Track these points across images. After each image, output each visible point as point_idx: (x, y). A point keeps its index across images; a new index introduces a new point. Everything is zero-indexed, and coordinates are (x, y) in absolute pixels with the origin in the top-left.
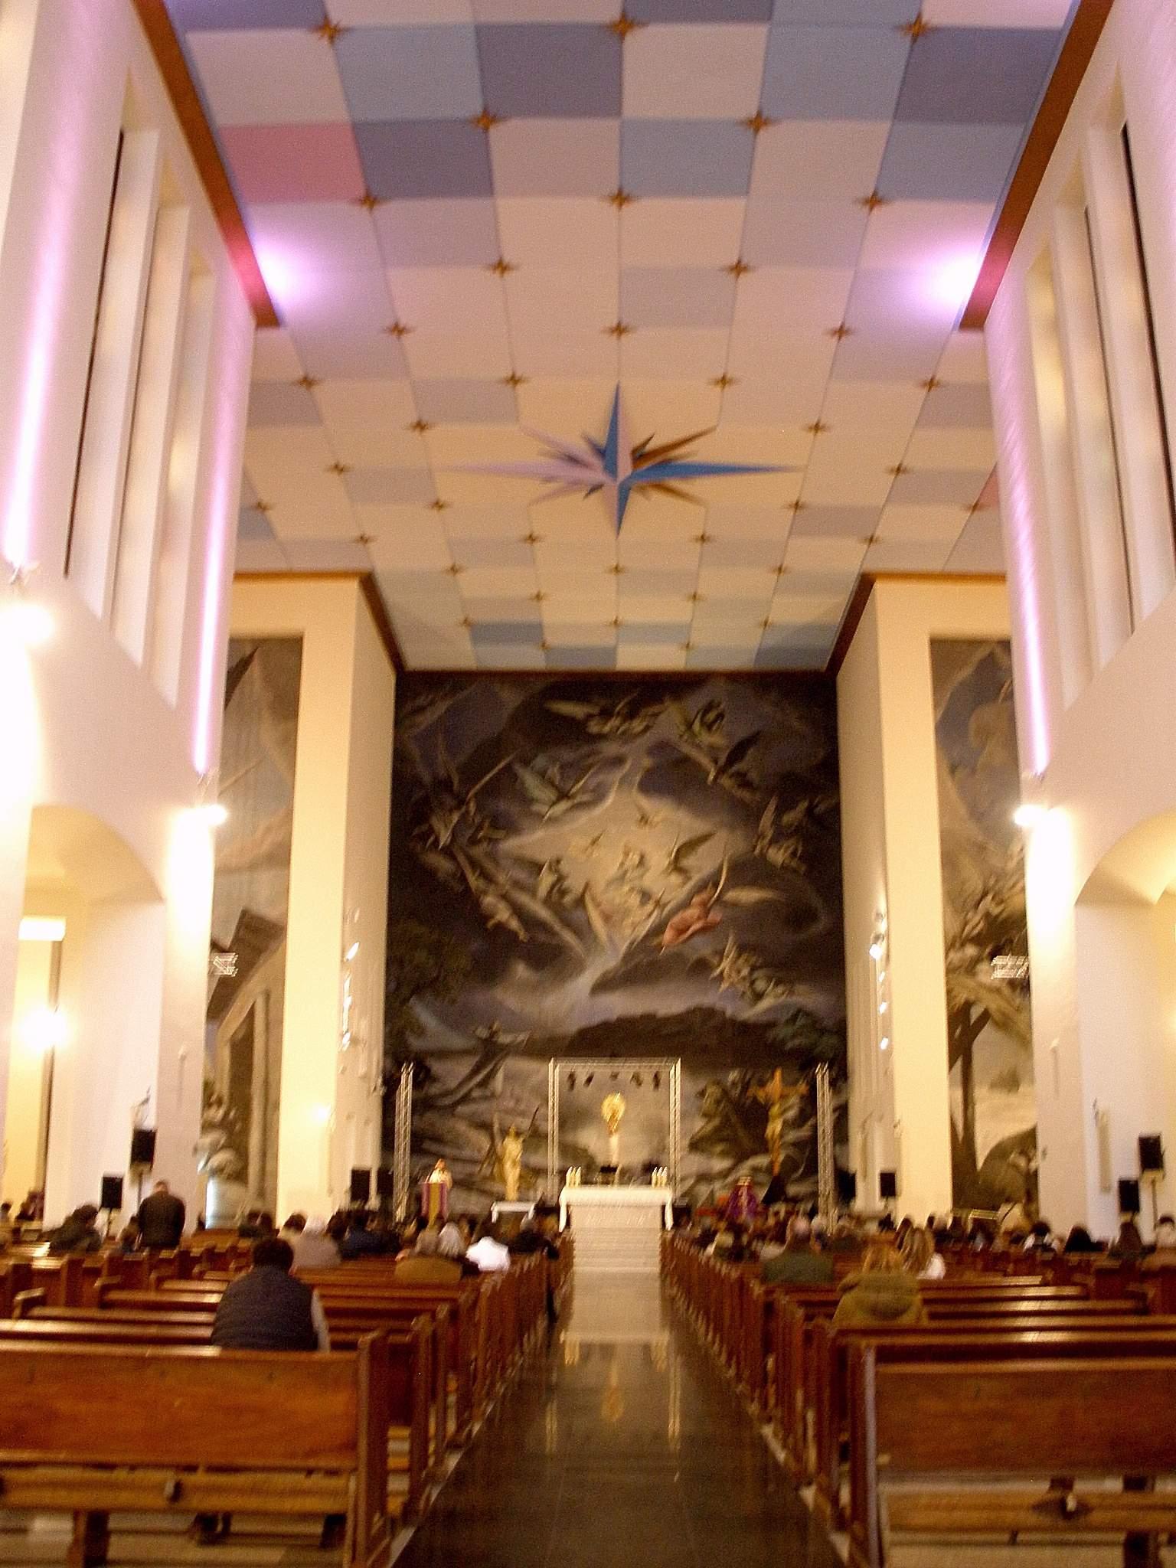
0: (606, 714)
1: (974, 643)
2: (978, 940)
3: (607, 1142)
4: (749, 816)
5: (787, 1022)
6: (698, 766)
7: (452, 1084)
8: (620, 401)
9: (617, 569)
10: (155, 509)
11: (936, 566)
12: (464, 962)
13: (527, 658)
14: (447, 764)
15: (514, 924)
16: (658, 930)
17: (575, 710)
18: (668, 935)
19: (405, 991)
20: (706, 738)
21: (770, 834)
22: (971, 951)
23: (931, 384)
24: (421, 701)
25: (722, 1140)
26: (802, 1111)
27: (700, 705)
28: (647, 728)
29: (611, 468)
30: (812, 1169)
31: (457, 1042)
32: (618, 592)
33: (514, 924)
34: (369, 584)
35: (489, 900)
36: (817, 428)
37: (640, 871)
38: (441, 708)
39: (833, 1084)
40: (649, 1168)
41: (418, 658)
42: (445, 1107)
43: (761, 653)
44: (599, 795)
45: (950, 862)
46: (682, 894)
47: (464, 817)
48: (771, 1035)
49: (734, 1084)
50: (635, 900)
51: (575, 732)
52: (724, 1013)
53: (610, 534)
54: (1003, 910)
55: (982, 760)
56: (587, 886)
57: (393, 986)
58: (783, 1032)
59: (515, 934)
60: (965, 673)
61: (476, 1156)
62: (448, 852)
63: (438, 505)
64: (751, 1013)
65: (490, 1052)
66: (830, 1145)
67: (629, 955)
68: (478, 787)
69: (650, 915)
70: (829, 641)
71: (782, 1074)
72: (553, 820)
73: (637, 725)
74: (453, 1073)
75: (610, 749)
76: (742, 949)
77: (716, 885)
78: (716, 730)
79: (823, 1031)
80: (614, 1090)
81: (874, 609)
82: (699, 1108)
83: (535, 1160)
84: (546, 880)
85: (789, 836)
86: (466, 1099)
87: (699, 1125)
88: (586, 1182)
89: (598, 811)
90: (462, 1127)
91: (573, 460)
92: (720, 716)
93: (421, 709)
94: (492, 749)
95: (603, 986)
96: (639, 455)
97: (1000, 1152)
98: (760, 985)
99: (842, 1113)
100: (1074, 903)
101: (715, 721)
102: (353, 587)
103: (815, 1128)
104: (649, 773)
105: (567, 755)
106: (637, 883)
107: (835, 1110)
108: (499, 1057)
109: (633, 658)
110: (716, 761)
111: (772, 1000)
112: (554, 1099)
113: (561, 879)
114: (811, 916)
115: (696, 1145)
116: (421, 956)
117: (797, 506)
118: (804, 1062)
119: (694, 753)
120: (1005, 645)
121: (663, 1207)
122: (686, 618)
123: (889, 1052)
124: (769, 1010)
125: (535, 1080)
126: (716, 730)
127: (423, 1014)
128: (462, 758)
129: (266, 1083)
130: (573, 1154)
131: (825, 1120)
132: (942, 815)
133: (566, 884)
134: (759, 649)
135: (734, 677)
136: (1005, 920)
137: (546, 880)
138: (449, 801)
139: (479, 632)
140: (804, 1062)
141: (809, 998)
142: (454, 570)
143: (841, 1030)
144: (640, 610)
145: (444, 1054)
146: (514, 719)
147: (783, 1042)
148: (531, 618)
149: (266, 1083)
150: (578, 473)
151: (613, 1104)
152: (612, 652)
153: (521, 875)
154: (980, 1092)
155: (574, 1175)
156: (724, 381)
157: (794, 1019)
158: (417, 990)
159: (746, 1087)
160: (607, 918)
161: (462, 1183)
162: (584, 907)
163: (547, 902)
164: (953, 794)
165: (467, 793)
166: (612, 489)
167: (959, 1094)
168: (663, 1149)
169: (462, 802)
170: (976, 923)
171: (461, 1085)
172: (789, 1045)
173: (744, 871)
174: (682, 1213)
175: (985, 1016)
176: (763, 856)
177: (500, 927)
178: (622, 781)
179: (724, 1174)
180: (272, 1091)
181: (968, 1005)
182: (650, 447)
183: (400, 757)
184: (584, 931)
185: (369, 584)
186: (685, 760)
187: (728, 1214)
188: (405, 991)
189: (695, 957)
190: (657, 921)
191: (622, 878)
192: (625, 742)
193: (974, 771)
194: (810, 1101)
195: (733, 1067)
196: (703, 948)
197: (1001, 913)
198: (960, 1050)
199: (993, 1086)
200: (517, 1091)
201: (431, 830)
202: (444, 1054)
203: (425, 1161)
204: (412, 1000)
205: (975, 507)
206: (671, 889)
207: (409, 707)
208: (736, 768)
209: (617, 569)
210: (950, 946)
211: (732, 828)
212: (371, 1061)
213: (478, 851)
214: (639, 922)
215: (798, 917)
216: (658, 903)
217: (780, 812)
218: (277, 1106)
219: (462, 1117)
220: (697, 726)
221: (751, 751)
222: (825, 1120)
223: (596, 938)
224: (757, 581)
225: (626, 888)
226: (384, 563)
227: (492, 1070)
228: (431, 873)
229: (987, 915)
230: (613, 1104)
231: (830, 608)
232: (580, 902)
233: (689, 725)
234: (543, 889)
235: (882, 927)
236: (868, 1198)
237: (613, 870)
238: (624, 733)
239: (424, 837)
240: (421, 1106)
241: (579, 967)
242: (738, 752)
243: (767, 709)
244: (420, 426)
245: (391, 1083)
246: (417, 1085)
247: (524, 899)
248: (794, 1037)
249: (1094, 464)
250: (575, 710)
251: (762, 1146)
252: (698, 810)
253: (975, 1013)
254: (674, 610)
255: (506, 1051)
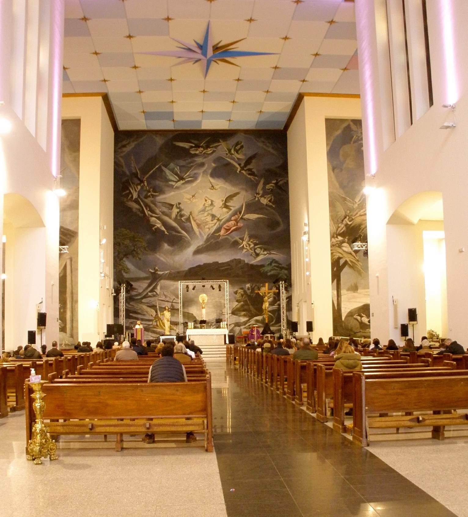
0: (197, 146)
1: (342, 121)
2: (343, 235)
3: (201, 311)
4: (253, 186)
5: (268, 264)
6: (234, 166)
7: (141, 291)
8: (210, 27)
9: (204, 91)
10: (342, 294)
11: (328, 91)
12: (144, 244)
13: (166, 125)
14: (135, 167)
15: (163, 228)
16: (218, 230)
17: (186, 145)
18: (222, 232)
19: (121, 255)
20: (236, 156)
21: (261, 192)
22: (340, 238)
23: (332, 22)
24: (124, 143)
25: (244, 311)
26: (274, 298)
27: (233, 144)
28: (214, 151)
29: (205, 54)
30: (278, 321)
31: (143, 275)
32: (204, 100)
33: (163, 228)
34: (106, 98)
35: (153, 219)
36: (286, 38)
37: (211, 207)
38: (133, 145)
39: (286, 289)
40: (219, 321)
41: (123, 126)
42: (137, 299)
43: (258, 123)
44: (195, 178)
45: (332, 205)
46: (227, 216)
47: (142, 187)
48: (262, 270)
49: (248, 289)
50: (209, 218)
51: (185, 153)
52: (245, 262)
53: (203, 78)
54: (352, 223)
55: (345, 166)
56: (191, 213)
57: (117, 254)
58: (267, 269)
59: (164, 232)
60: (339, 132)
61: (151, 318)
62: (136, 201)
63: (135, 67)
64: (254, 261)
65: (155, 278)
66: (285, 312)
67: (208, 240)
68: (148, 175)
69: (215, 224)
70: (285, 119)
71: (268, 285)
72: (177, 188)
73: (209, 151)
74: (141, 287)
75: (199, 160)
76: (251, 237)
77: (240, 213)
78: (240, 153)
79: (282, 268)
80: (204, 292)
81: (304, 107)
82: (235, 298)
83: (174, 319)
84: (175, 211)
85: (268, 194)
86: (145, 297)
87: (235, 304)
88: (195, 327)
89: (194, 184)
90: (145, 307)
91: (190, 50)
92: (242, 147)
93: (124, 146)
94: (153, 161)
95: (197, 252)
96: (216, 48)
97: (350, 314)
98: (258, 251)
99: (289, 299)
100: (386, 223)
101: (239, 149)
102: (100, 99)
103: (279, 305)
104: (215, 169)
105: (182, 162)
106: (210, 212)
107: (287, 299)
108: (158, 280)
109: (208, 125)
110: (240, 165)
111: (263, 256)
112: (181, 296)
113: (181, 210)
114: (277, 224)
115: (234, 313)
116: (127, 242)
117: (276, 68)
118: (275, 281)
119: (232, 161)
120: (358, 123)
121: (225, 336)
122: (230, 110)
123: (309, 276)
124: (262, 260)
125: (172, 288)
126: (240, 153)
127: (128, 264)
128: (141, 165)
129: (72, 293)
130: (188, 316)
131: (283, 303)
132: (329, 187)
133: (183, 212)
134: (258, 121)
135: (246, 132)
136: (353, 226)
137: (175, 211)
138: (137, 181)
139: (148, 115)
140: (275, 281)
141: (277, 256)
142: (140, 92)
143: (289, 268)
144: (212, 107)
145: (138, 279)
146: (161, 149)
147: (267, 272)
148: (168, 110)
149: (72, 293)
150: (192, 55)
151: (203, 297)
152: (200, 122)
153: (165, 209)
154: (343, 292)
155: (191, 324)
156: (251, 20)
157: (271, 264)
158: (126, 255)
159: (253, 290)
160: (198, 225)
161: (147, 329)
162: (190, 222)
163: (175, 220)
164: (334, 179)
165: (144, 178)
166: (204, 61)
167: (335, 292)
168: (222, 314)
169: (142, 182)
170: (342, 228)
171: (144, 291)
172: (269, 274)
173: (251, 207)
174: (232, 339)
175: (346, 263)
176: (259, 200)
177: (158, 229)
178: (204, 172)
179: (245, 323)
180: (74, 296)
181: (339, 258)
182: (220, 45)
183: (117, 164)
184: (190, 231)
185: (106, 98)
186: (229, 164)
187: (246, 338)
188: (121, 255)
189: (233, 240)
190: (219, 226)
191: (204, 210)
192: (205, 157)
193: (342, 170)
194: (277, 295)
195: (249, 282)
196: (236, 237)
197: (351, 224)
198: (336, 276)
199: (348, 290)
200: (165, 293)
201: (130, 193)
202: (138, 279)
203: (132, 320)
204: (124, 259)
205: (345, 69)
206: (224, 214)
207: (120, 145)
208: (248, 167)
209: (204, 91)
210: (332, 237)
211: (246, 191)
212: (110, 283)
213: (148, 201)
214: (211, 227)
215: (272, 224)
216: (218, 220)
217: (265, 184)
218: (77, 302)
219: (144, 303)
220: (233, 151)
221: (254, 161)
222: (283, 303)
223: (195, 233)
224: (260, 96)
225: (206, 214)
226: (112, 90)
227: (156, 284)
228: (130, 209)
229: (346, 225)
230: (203, 297)
231: (286, 106)
232: (188, 220)
233: (230, 151)
234: (174, 216)
235: (306, 229)
236: (302, 331)
237: (201, 207)
238: (204, 153)
239: (127, 195)
240: (129, 299)
241: (188, 244)
242: (248, 161)
243: (260, 144)
244: (130, 37)
245: (117, 291)
246: (127, 291)
247: (166, 218)
248: (270, 271)
249: (399, 58)
250: (186, 145)
251: (260, 311)
252: (234, 184)
253: (342, 262)
254: (224, 106)
255: (161, 277)
